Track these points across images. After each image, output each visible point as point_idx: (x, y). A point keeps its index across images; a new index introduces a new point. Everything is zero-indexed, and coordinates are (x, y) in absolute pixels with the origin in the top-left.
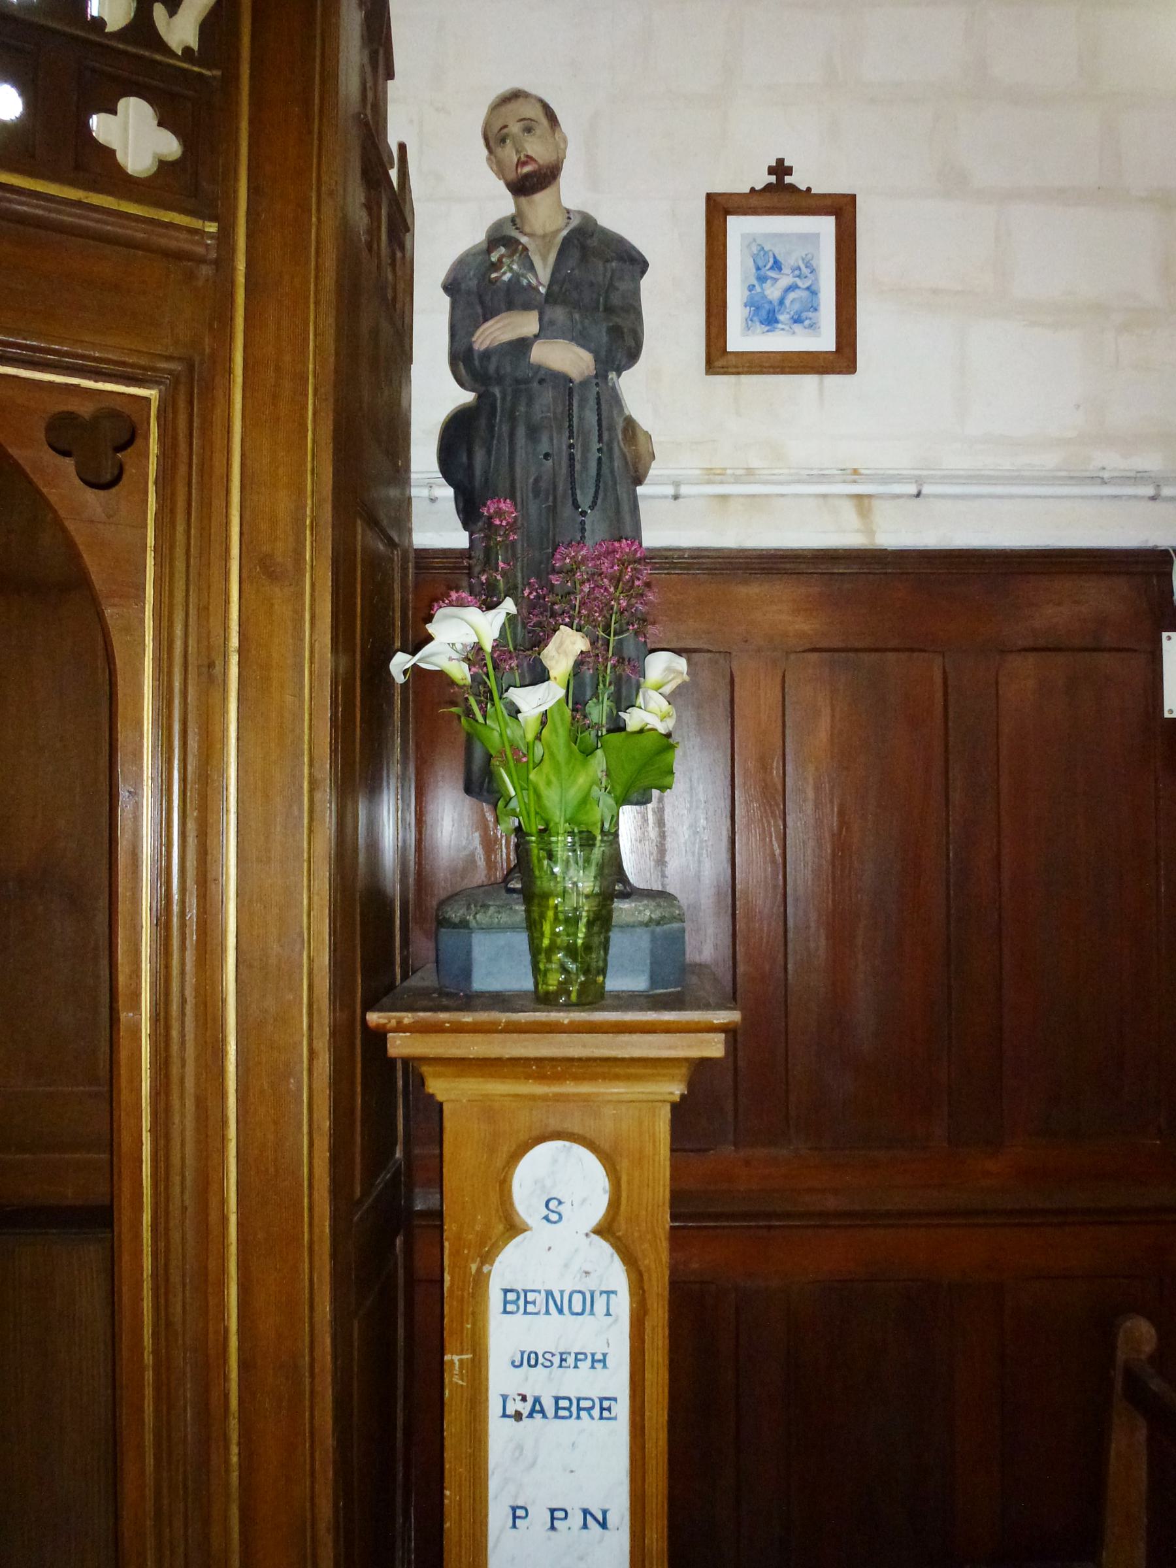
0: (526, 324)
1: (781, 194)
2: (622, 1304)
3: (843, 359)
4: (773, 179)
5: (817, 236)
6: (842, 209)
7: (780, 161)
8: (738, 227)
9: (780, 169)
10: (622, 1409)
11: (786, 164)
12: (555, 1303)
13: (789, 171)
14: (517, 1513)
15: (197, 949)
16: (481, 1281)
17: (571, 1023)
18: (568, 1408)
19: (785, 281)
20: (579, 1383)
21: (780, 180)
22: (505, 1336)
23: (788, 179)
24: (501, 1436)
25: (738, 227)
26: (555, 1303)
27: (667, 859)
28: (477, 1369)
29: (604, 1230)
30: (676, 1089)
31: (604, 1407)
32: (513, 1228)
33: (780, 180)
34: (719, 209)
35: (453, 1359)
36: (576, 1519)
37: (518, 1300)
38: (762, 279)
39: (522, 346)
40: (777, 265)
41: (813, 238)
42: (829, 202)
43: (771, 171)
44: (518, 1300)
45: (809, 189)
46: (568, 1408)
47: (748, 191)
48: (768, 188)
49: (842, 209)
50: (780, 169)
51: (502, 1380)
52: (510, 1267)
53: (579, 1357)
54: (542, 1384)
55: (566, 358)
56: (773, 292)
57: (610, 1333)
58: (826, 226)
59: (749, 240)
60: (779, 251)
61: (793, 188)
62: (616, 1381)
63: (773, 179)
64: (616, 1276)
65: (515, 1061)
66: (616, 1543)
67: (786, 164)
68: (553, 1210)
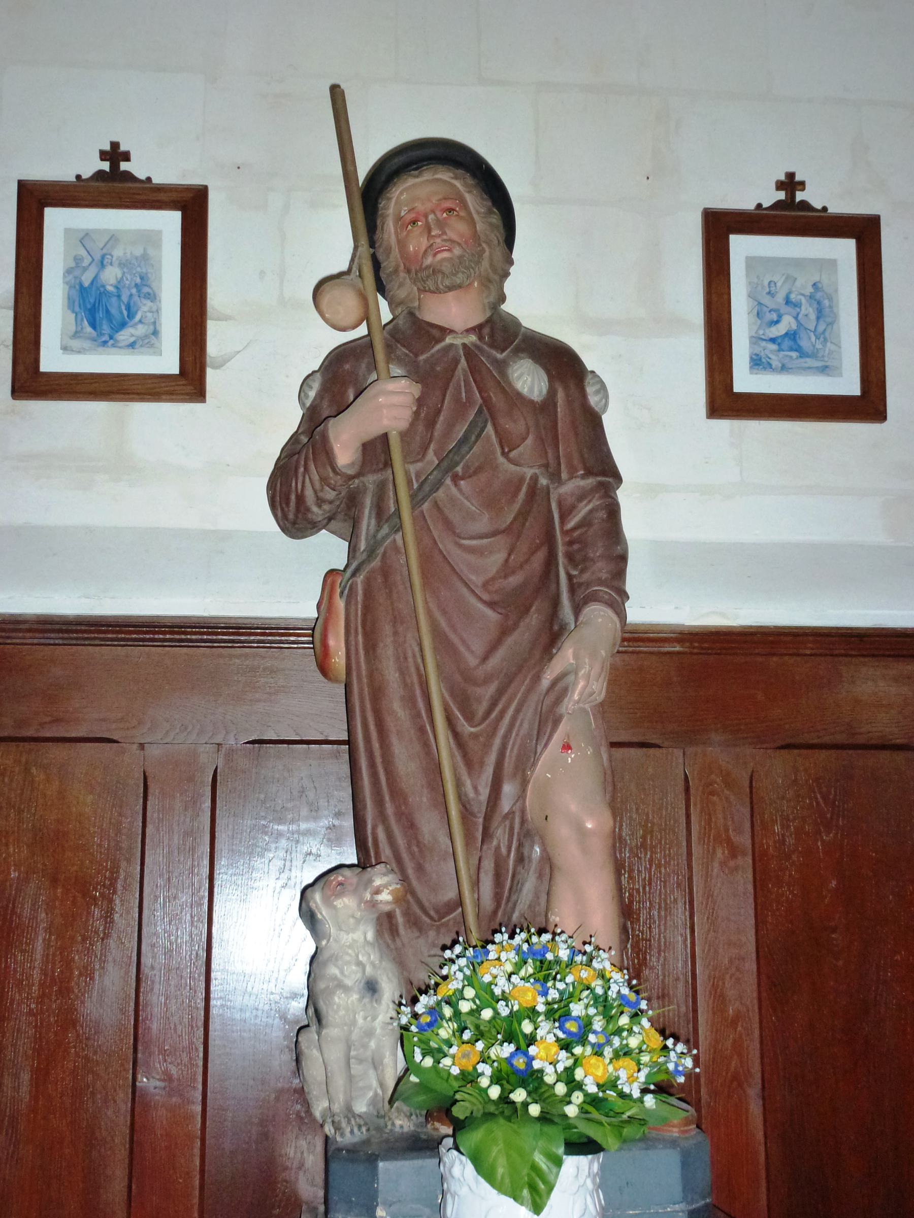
1: (792, 215)
3: (725, 402)
4: (106, 166)
5: (833, 263)
6: (865, 232)
7: (115, 145)
8: (57, 221)
9: (115, 154)
11: (123, 148)
13: (802, 185)
15: (506, 691)
21: (115, 166)
23: (124, 166)
25: (57, 221)
33: (115, 166)
34: (719, 227)
41: (153, 238)
42: (175, 196)
43: (780, 186)
45: (78, 177)
47: (819, 207)
48: (100, 175)
49: (865, 232)
50: (115, 154)
58: (844, 250)
59: (752, 263)
61: (129, 177)
63: (781, 195)
66: (666, 1179)
67: (123, 148)
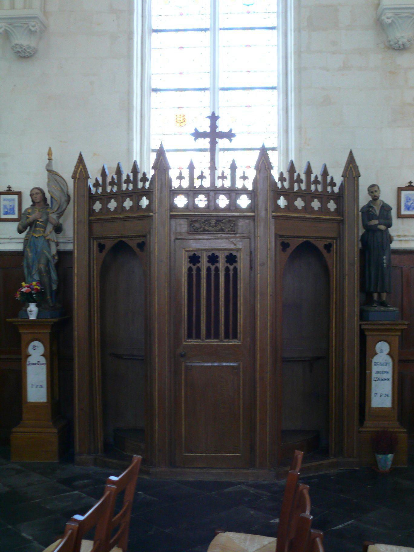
0: (376, 222)
2: (391, 364)
8: (404, 193)
10: (391, 379)
12: (381, 364)
14: (376, 394)
16: (371, 362)
17: (192, 274)
18: (383, 379)
19: (411, 202)
20: (385, 376)
22: (374, 369)
24: (374, 383)
26: (381, 364)
27: (216, 166)
28: (371, 373)
29: (389, 354)
30: (399, 333)
31: (388, 379)
32: (376, 354)
35: (368, 372)
36: (384, 395)
37: (376, 364)
38: (407, 202)
39: (376, 225)
40: (410, 199)
44: (376, 364)
46: (383, 379)
48: (408, 186)
51: (374, 375)
52: (375, 359)
53: (385, 372)
54: (379, 376)
55: (382, 227)
56: (409, 204)
57: (389, 369)
60: (410, 196)
62: (390, 376)
64: (390, 360)
65: (374, 329)
68: (381, 351)
